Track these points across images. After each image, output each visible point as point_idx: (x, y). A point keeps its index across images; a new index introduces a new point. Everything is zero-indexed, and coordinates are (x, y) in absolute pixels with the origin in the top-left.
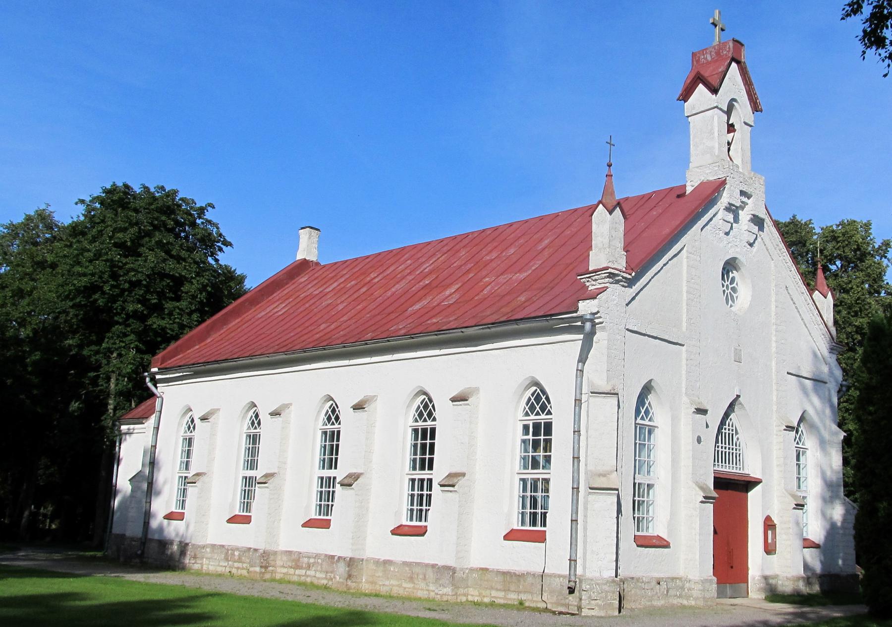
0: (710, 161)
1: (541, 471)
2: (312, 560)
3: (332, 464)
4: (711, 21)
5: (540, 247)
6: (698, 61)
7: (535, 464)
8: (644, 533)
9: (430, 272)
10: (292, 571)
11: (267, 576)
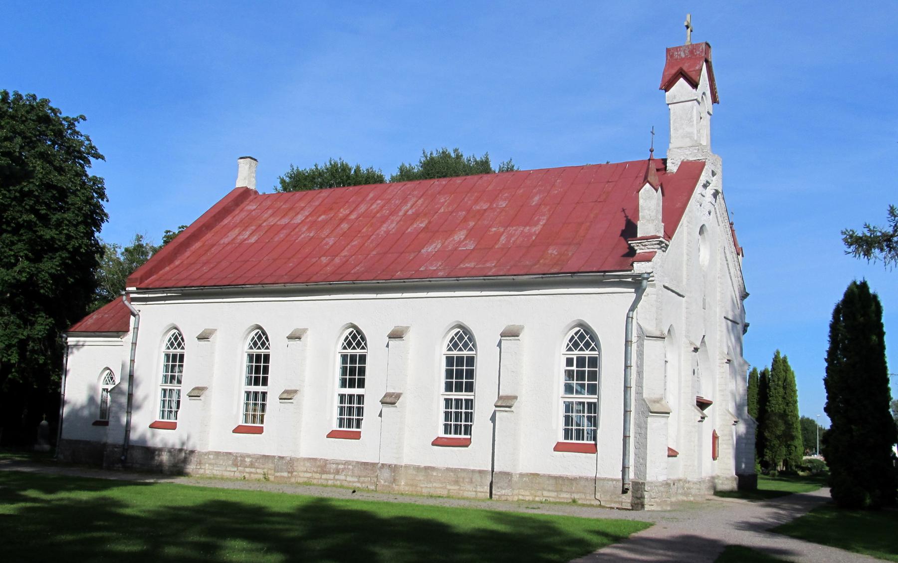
0: (690, 144)
1: (574, 395)
2: (341, 467)
4: (686, 24)
6: (672, 56)
10: (317, 476)
11: (293, 480)
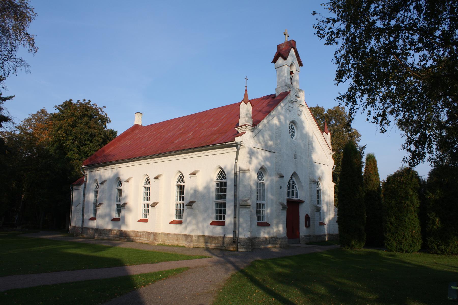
1: (223, 200)
2: (142, 234)
3: (148, 199)
5: (222, 118)
7: (221, 198)
8: (261, 222)
9: (183, 128)
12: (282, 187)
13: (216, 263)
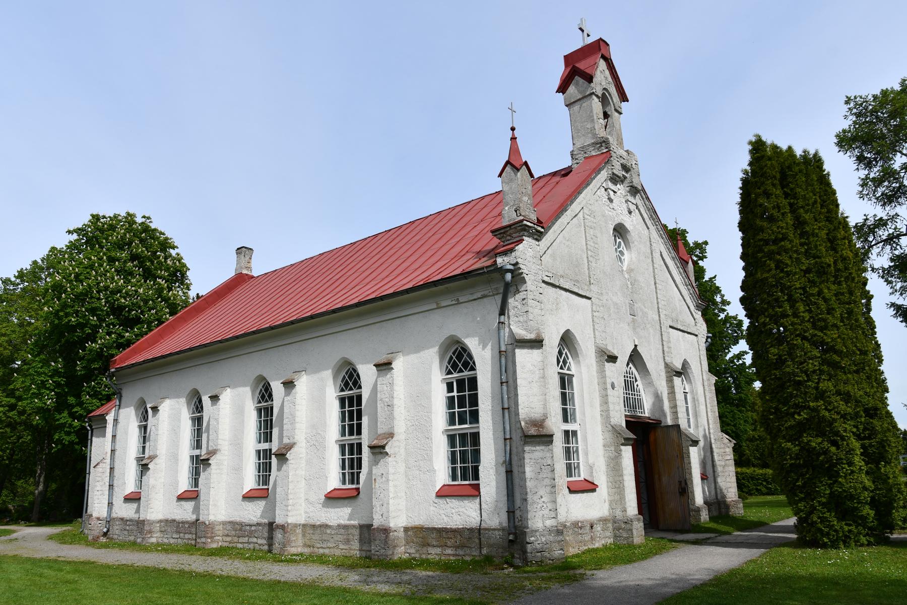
2: (253, 528)
12: (616, 385)
13: (174, 248)
